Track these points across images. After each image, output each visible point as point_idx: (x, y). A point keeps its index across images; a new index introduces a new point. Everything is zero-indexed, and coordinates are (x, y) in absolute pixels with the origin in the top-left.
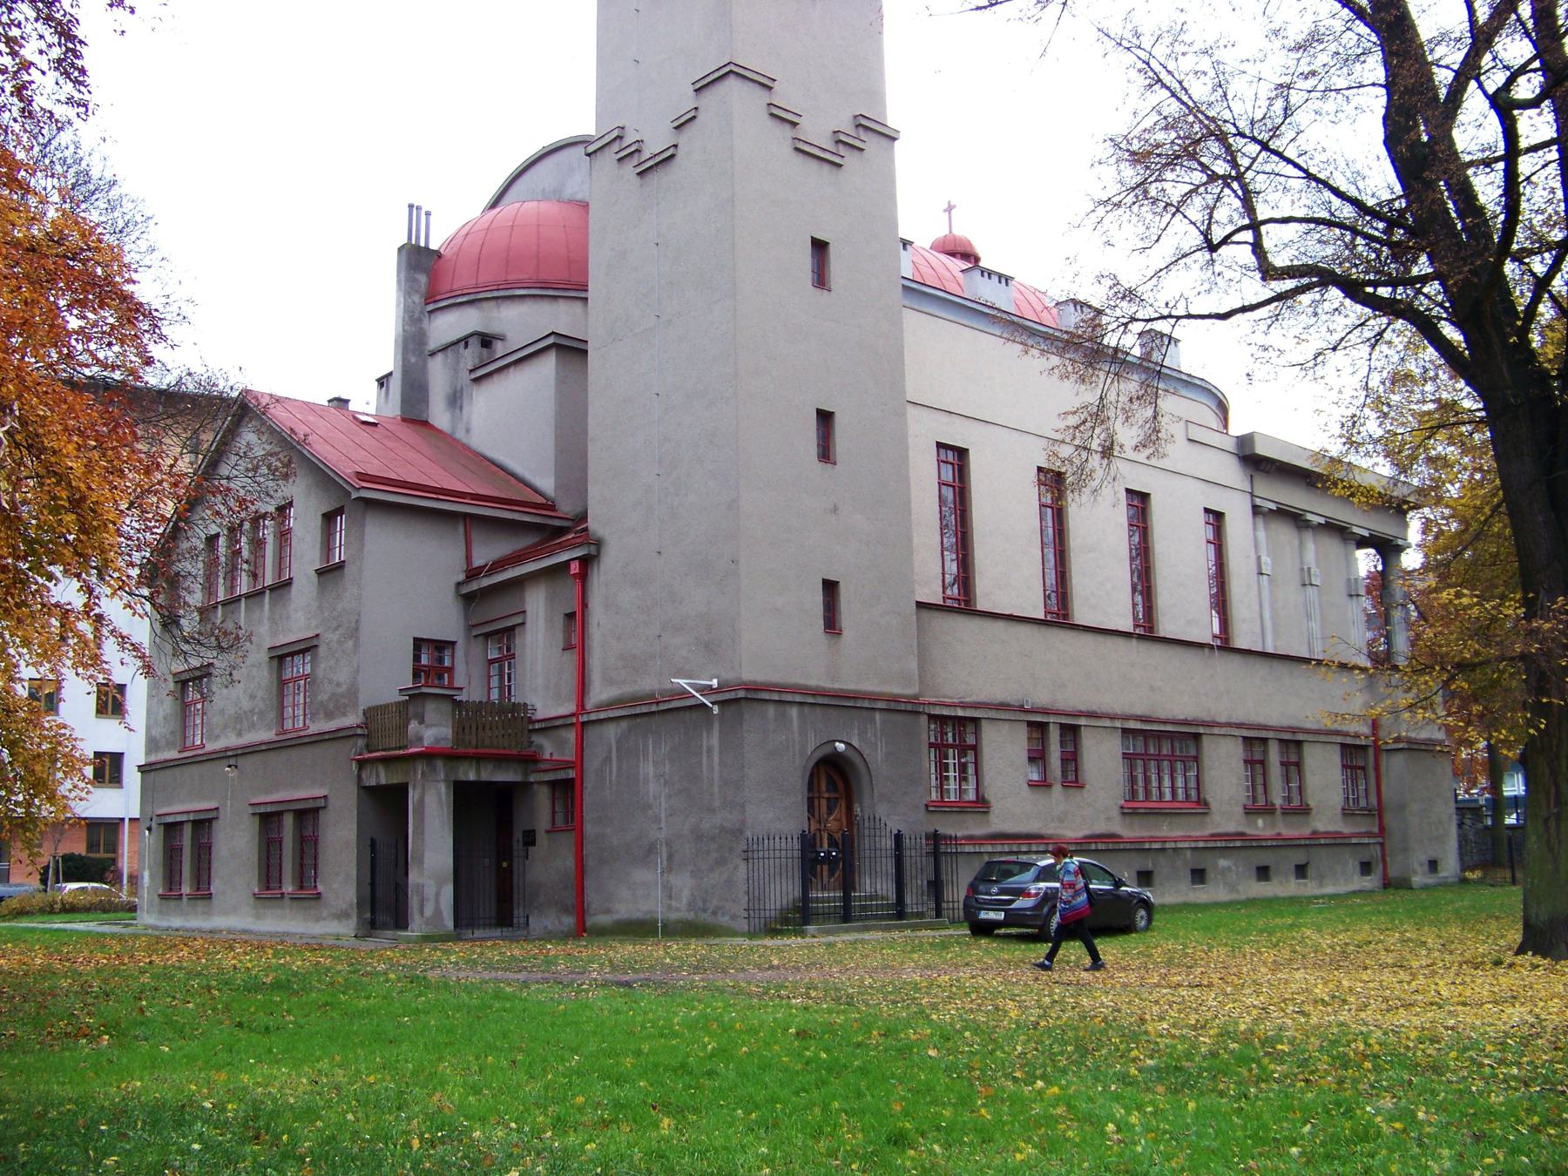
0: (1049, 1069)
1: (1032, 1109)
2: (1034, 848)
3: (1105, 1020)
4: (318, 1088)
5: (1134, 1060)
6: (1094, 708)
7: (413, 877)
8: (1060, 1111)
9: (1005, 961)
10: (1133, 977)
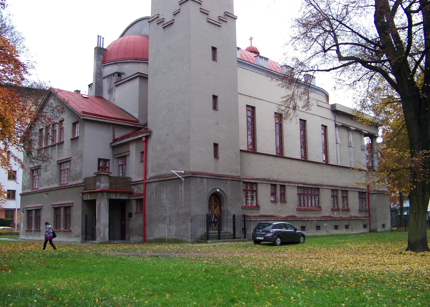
0: (275, 281)
1: (270, 292)
2: (272, 219)
3: (291, 268)
4: (70, 285)
5: (299, 279)
6: (290, 180)
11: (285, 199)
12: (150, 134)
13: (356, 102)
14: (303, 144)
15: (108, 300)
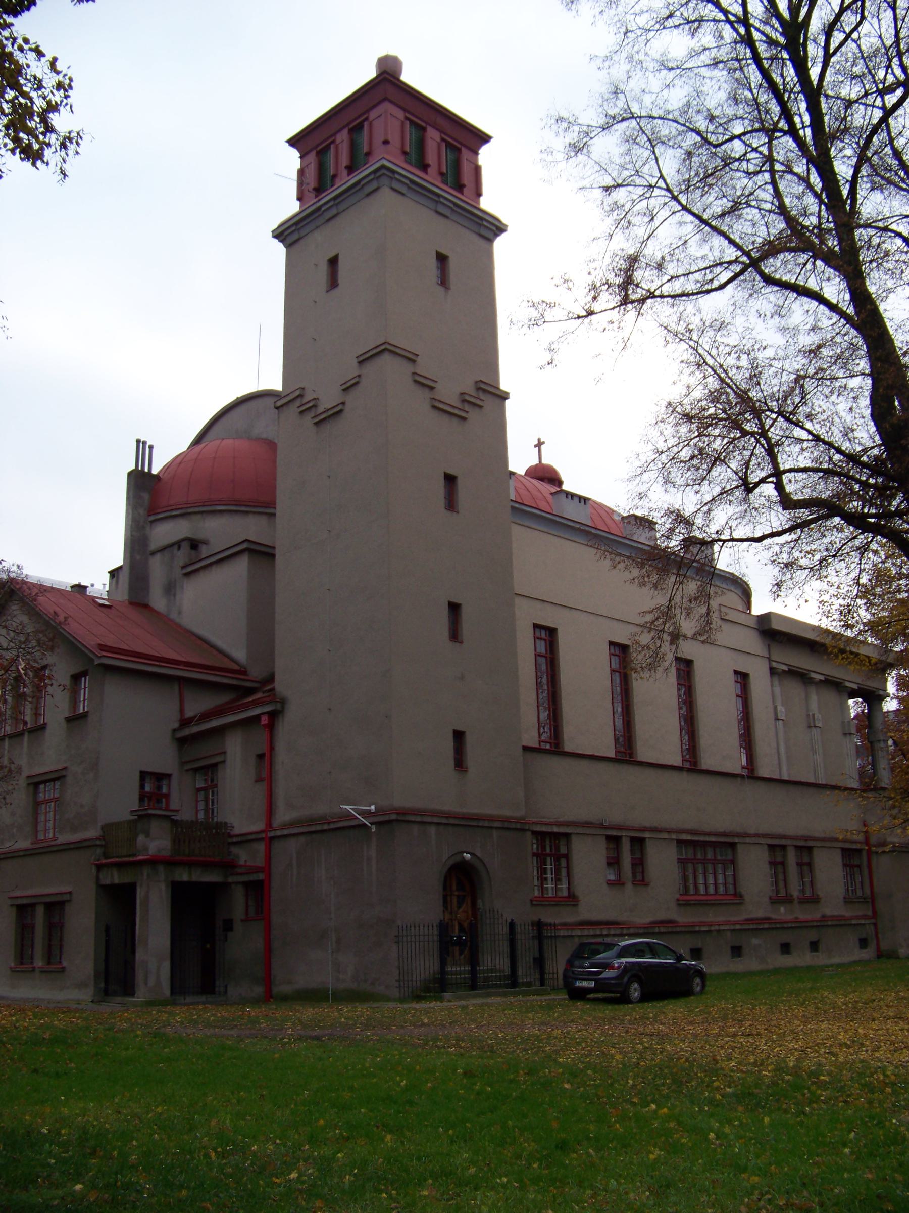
2: (612, 932)
3: (687, 1060)
5: (718, 1088)
7: (140, 955)
8: (672, 1125)
9: (601, 1018)
10: (699, 1029)
12: (283, 707)
13: (829, 612)
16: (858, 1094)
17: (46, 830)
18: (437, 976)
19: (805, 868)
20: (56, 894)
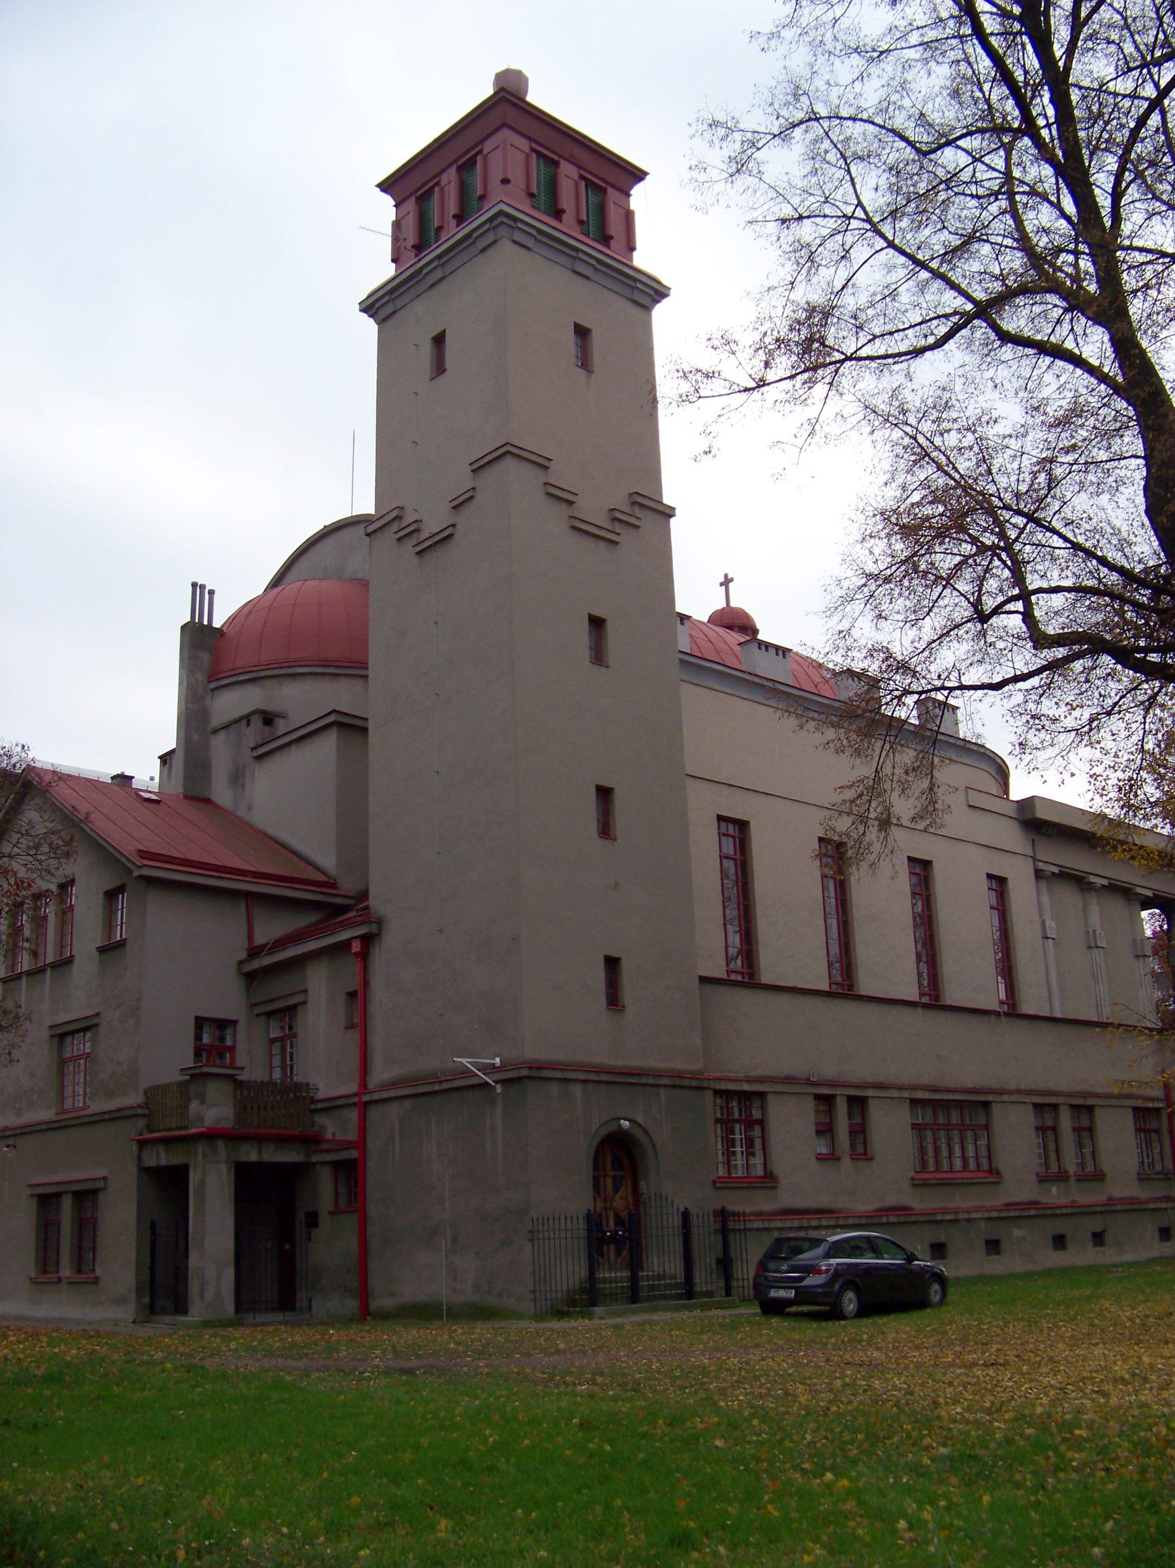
0: (838, 1460)
1: (821, 1504)
2: (824, 1223)
3: (897, 1405)
4: (82, 1494)
5: (927, 1448)
6: (881, 1078)
7: (194, 1260)
11: (868, 1145)
12: (380, 930)
13: (1103, 789)
14: (922, 947)
15: (223, 1552)
16: (1126, 1458)
17: (74, 1096)
18: (584, 1285)
19: (1085, 1134)
20: (86, 1180)
